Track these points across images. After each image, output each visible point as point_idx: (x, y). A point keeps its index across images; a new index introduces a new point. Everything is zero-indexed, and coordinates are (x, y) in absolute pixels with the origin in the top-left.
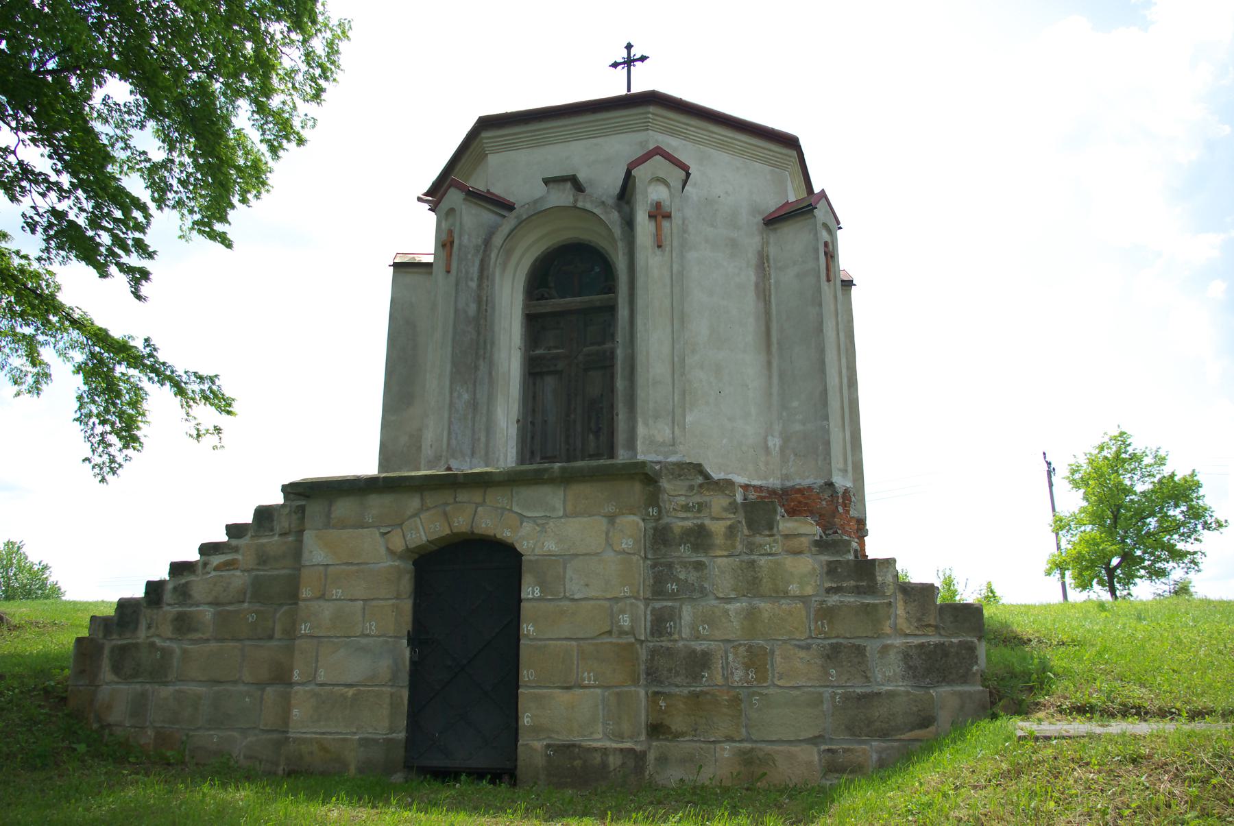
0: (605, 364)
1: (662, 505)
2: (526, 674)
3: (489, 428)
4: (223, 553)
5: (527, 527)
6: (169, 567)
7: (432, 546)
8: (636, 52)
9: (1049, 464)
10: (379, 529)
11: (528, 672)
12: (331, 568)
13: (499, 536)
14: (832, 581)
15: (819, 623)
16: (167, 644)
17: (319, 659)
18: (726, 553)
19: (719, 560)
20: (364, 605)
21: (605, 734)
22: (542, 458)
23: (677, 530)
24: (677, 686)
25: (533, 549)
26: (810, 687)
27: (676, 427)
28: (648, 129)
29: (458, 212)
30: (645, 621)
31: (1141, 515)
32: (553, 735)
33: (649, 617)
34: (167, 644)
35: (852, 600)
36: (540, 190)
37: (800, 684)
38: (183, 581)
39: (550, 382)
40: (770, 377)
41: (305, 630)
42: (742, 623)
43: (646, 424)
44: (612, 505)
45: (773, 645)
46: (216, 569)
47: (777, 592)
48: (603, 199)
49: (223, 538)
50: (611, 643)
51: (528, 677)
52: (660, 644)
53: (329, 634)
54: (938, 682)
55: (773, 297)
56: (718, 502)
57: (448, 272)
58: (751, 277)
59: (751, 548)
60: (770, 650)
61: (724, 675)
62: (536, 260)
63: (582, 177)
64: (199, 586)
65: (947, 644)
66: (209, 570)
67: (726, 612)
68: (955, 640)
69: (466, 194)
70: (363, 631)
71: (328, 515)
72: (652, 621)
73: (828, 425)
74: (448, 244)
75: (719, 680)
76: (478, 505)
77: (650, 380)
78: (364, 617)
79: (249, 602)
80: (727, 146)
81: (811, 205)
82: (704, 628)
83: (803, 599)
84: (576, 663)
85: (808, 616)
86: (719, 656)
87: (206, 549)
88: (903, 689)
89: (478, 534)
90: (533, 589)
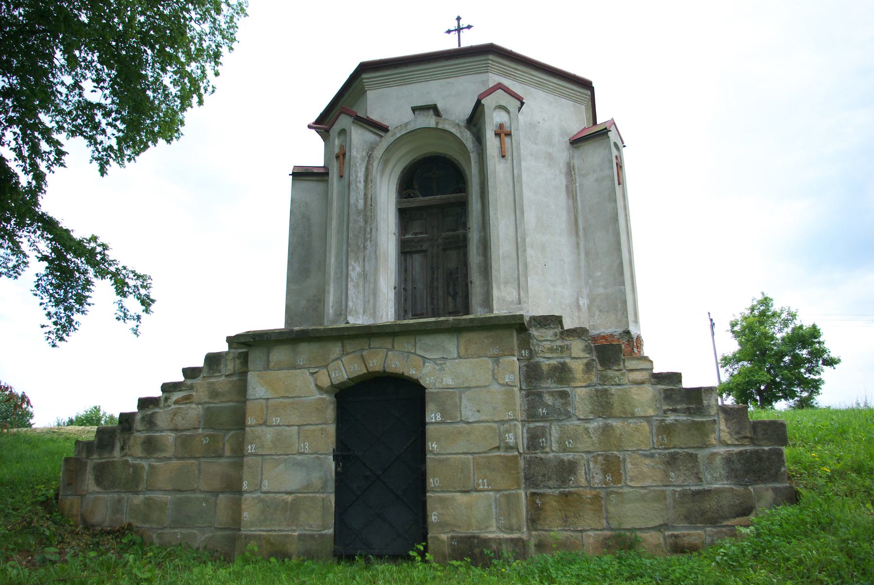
0: (461, 245)
1: (532, 348)
2: (432, 482)
3: (375, 293)
4: (181, 390)
5: (429, 366)
6: (137, 402)
7: (351, 382)
8: (463, 23)
9: (711, 320)
10: (309, 370)
11: (434, 480)
12: (271, 401)
13: (406, 374)
14: (669, 404)
15: (660, 437)
16: (138, 461)
17: (264, 472)
18: (584, 384)
19: (578, 390)
20: (299, 429)
21: (498, 527)
22: (413, 315)
23: (545, 368)
24: (550, 488)
25: (434, 384)
26: (654, 486)
27: (521, 290)
28: (488, 72)
29: (348, 134)
30: (522, 438)
31: (781, 355)
32: (456, 529)
33: (525, 435)
34: (138, 461)
35: (685, 418)
36: (409, 115)
37: (647, 484)
38: (149, 412)
39: (417, 259)
40: (579, 254)
41: (251, 450)
42: (600, 438)
43: (499, 289)
44: (496, 348)
45: (625, 455)
46: (175, 403)
47: (625, 413)
48: (457, 122)
49: (180, 378)
50: (500, 456)
51: (434, 484)
52: (535, 455)
53: (271, 452)
54: (754, 481)
55: (578, 196)
56: (577, 346)
57: (341, 177)
58: (562, 181)
59: (604, 379)
60: (623, 458)
61: (586, 478)
62: (405, 169)
63: (439, 106)
64: (162, 417)
65: (760, 451)
66: (170, 404)
67: (586, 429)
68: (766, 448)
69: (355, 119)
70: (298, 450)
71: (268, 361)
72: (528, 438)
73: (625, 288)
74: (341, 156)
75: (583, 481)
76: (388, 350)
77: (501, 255)
78: (299, 438)
79: (203, 429)
80: (542, 85)
81: (606, 128)
82: (569, 443)
83: (647, 419)
84: (472, 472)
85: (651, 432)
86: (583, 465)
87: (168, 388)
88: (727, 486)
89: (389, 373)
90: (435, 414)
